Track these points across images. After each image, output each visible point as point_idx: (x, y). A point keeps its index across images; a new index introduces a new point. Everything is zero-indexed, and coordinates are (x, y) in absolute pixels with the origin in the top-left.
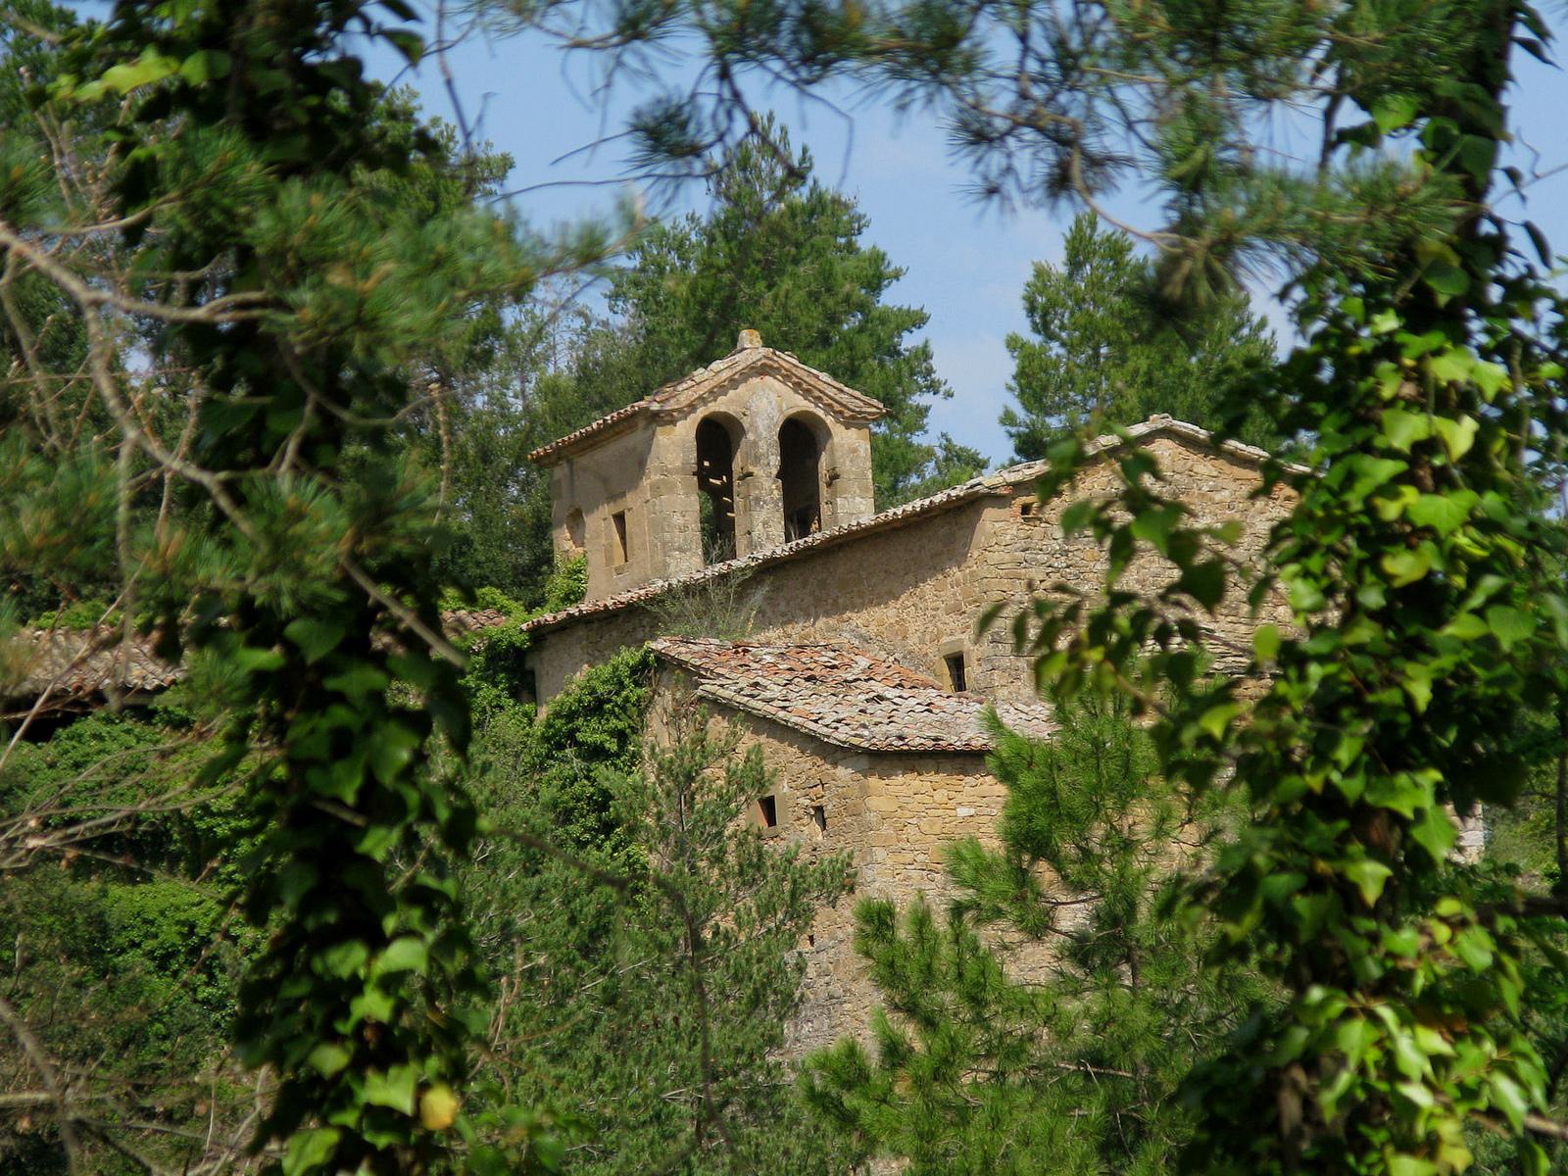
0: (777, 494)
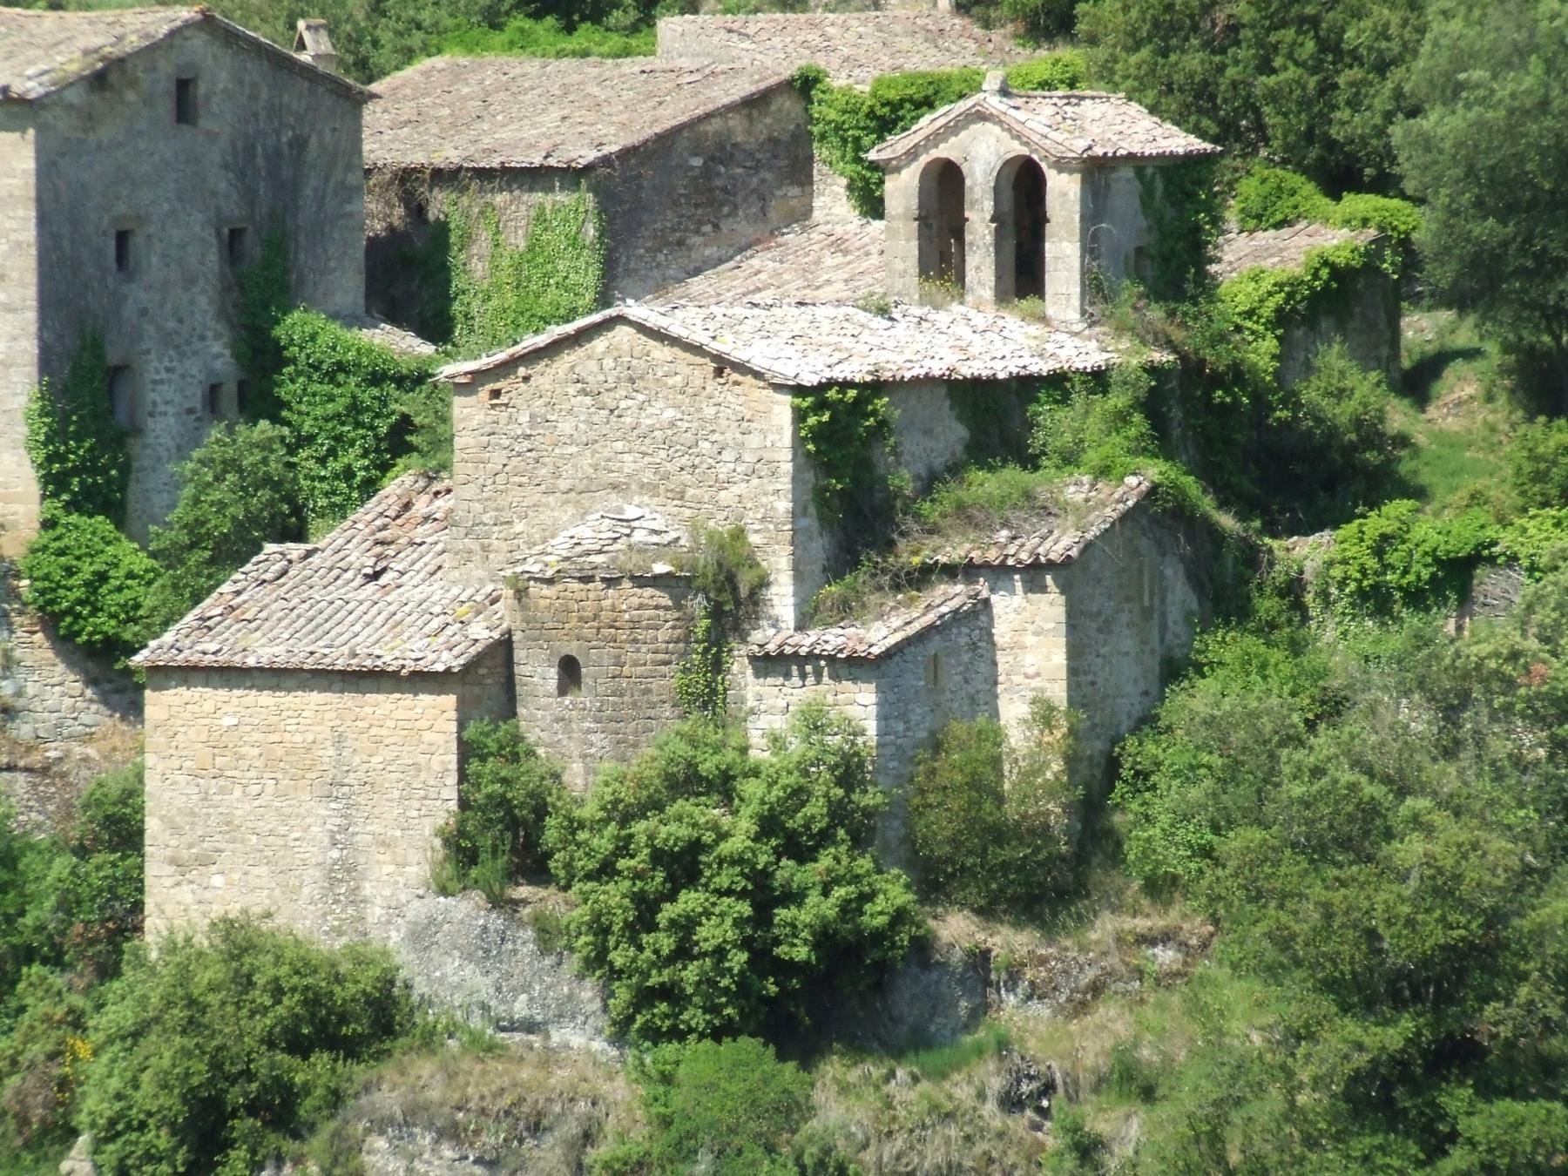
0: (989, 239)
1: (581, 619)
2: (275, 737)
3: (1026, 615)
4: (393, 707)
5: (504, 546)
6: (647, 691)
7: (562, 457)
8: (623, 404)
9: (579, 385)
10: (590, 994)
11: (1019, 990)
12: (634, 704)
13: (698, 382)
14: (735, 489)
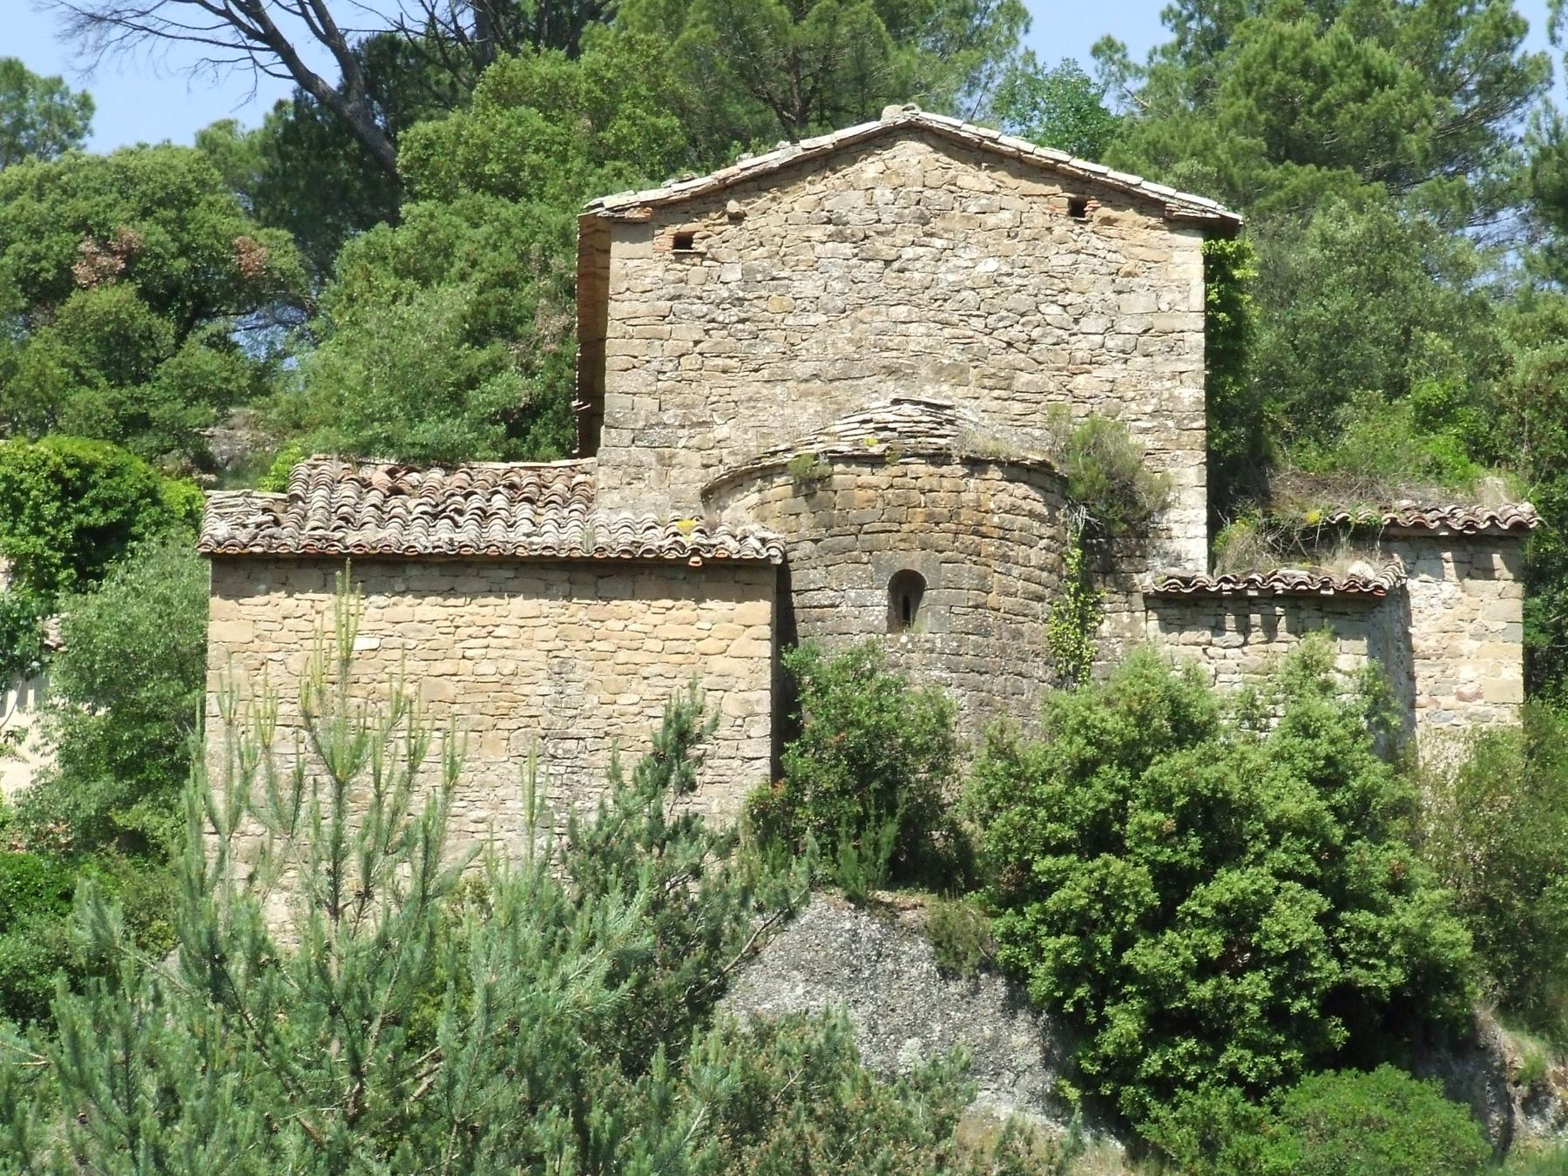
1: (931, 518)
2: (446, 667)
3: (1460, 610)
4: (658, 619)
5: (697, 459)
6: (1016, 635)
7: (800, 328)
8: (909, 253)
9: (831, 228)
10: (1025, 1039)
11: (1549, 1112)
12: (1003, 650)
13: (1041, 221)
14: (1104, 373)
